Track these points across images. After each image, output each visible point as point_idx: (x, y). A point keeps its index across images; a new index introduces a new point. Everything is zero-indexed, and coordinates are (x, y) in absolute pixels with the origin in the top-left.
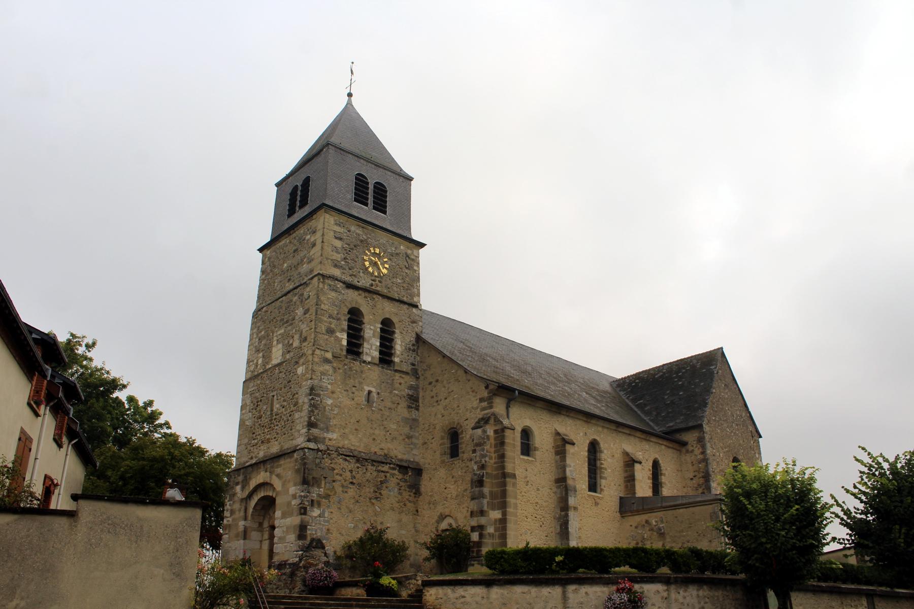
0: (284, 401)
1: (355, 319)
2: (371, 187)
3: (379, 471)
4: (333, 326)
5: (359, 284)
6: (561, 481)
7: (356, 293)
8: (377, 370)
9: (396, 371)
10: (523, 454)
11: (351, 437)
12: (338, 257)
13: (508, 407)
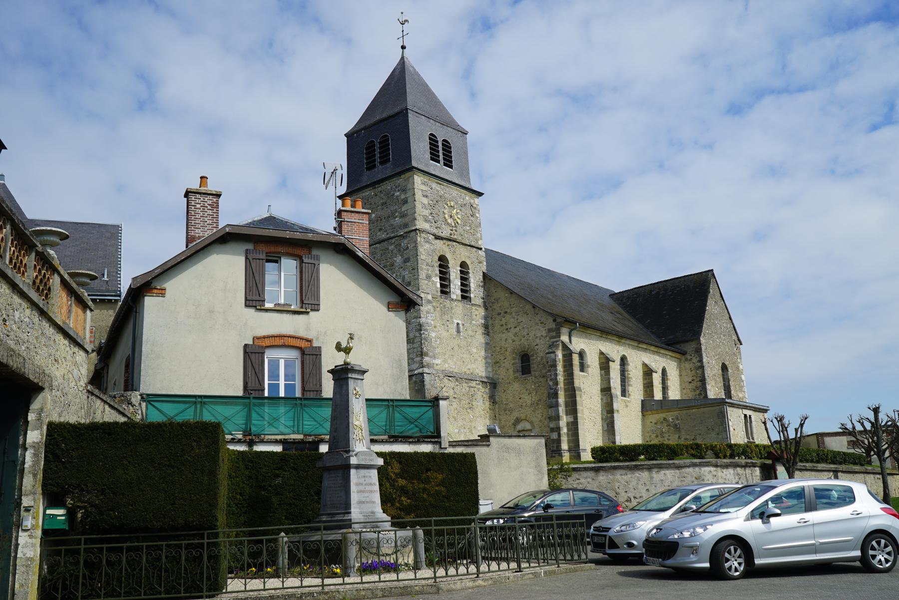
1: (443, 262)
5: (442, 235)
6: (606, 390)
7: (442, 242)
8: (460, 304)
9: (473, 305)
11: (449, 361)
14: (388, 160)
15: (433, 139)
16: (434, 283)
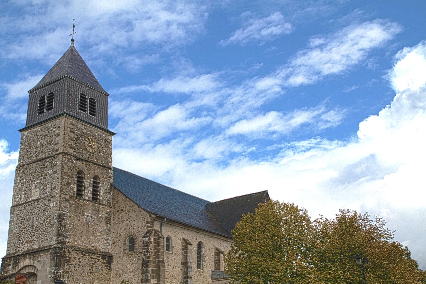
0: (41, 220)
2: (88, 100)
3: (92, 258)
4: (70, 181)
5: (82, 158)
6: (185, 263)
8: (91, 203)
10: (167, 250)
12: (72, 143)
13: (161, 227)
14: (52, 108)
15: (83, 98)
16: (73, 189)
